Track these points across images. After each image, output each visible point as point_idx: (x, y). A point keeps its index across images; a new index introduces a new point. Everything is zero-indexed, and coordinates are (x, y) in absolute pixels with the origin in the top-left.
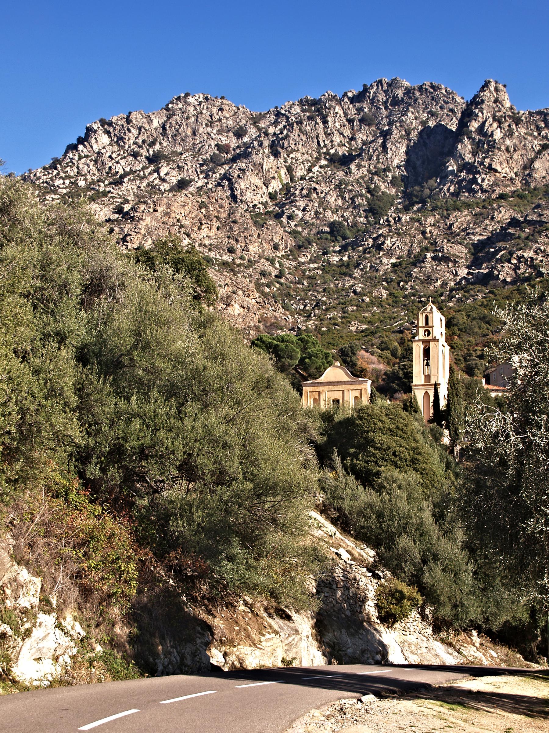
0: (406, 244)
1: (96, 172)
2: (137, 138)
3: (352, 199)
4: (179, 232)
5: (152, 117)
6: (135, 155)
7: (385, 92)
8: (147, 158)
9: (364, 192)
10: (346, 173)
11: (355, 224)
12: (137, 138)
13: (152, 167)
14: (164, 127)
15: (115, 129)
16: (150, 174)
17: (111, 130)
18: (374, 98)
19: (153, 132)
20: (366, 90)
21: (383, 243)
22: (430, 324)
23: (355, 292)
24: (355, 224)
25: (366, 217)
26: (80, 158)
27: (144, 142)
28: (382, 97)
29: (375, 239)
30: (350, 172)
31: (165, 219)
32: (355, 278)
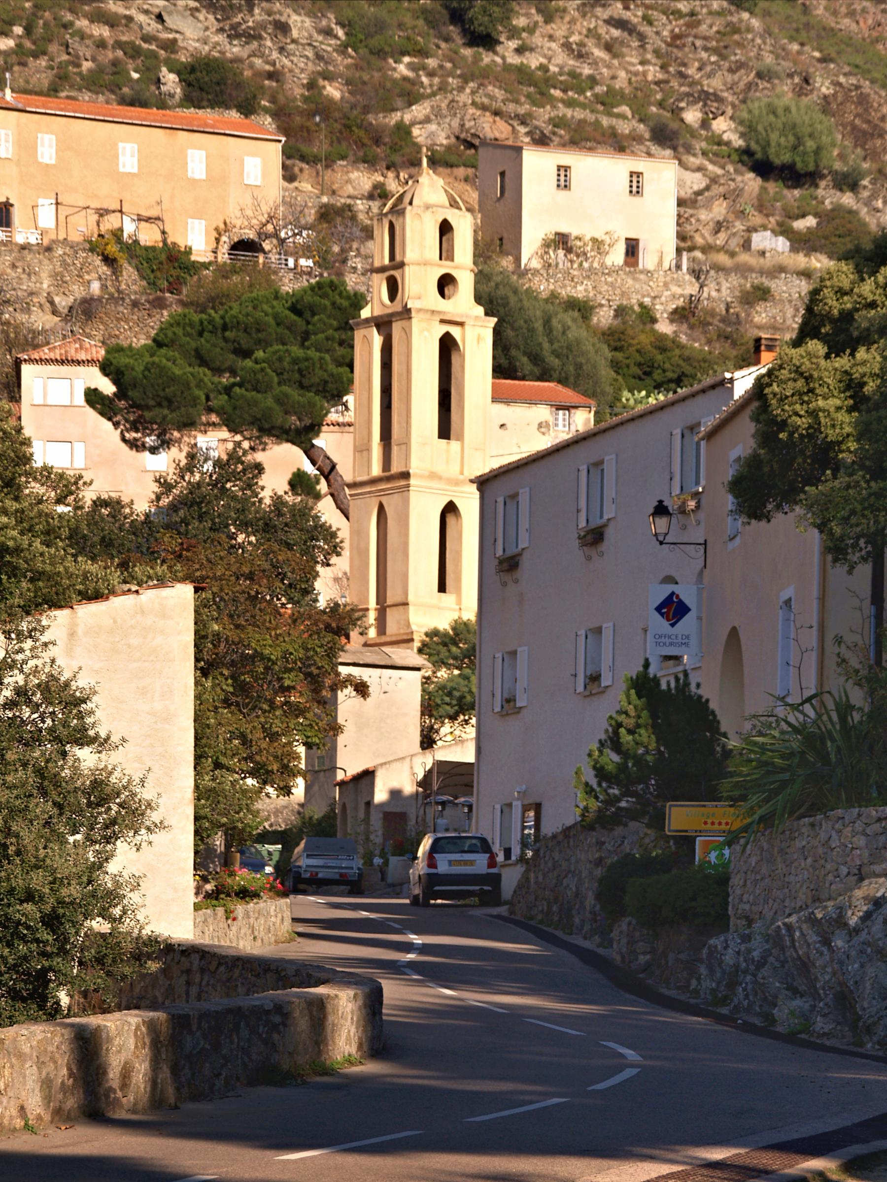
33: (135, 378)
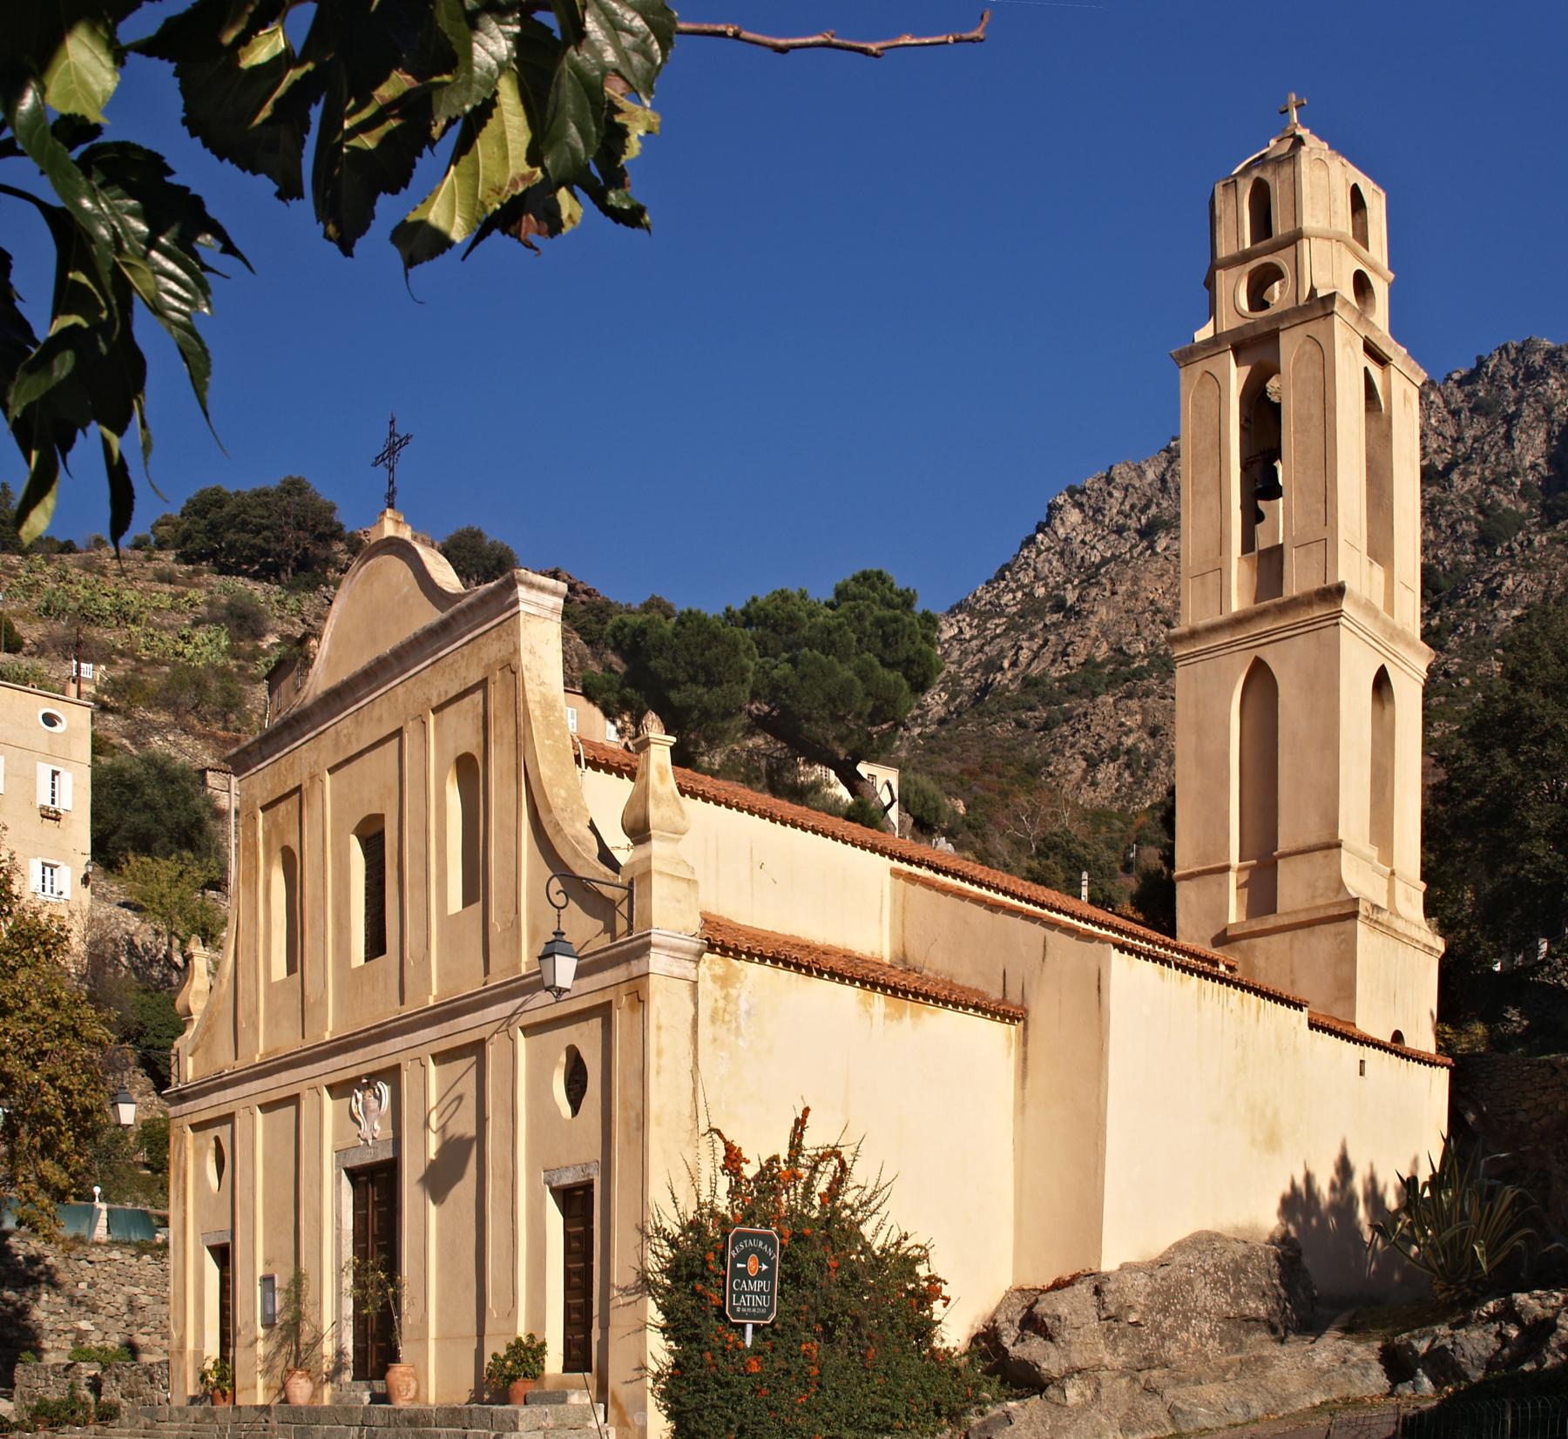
0: (1540, 583)
1: (1062, 570)
2: (1122, 503)
3: (1452, 527)
4: (1153, 622)
5: (1145, 466)
6: (1120, 531)
7: (1513, 362)
8: (1137, 531)
9: (1472, 512)
10: (1444, 488)
11: (1456, 566)
12: (1122, 503)
13: (1145, 544)
14: (1163, 480)
15: (1089, 497)
16: (1141, 553)
17: (1084, 500)
18: (1494, 374)
19: (1147, 488)
20: (1481, 363)
21: (1500, 586)
22: (1280, 228)
23: (1446, 674)
24: (1456, 566)
25: (1476, 553)
26: (1039, 553)
27: (1133, 507)
28: (1508, 371)
29: (1486, 583)
30: (1451, 486)
31: (1130, 604)
32: (1449, 651)
33: (662, 637)
